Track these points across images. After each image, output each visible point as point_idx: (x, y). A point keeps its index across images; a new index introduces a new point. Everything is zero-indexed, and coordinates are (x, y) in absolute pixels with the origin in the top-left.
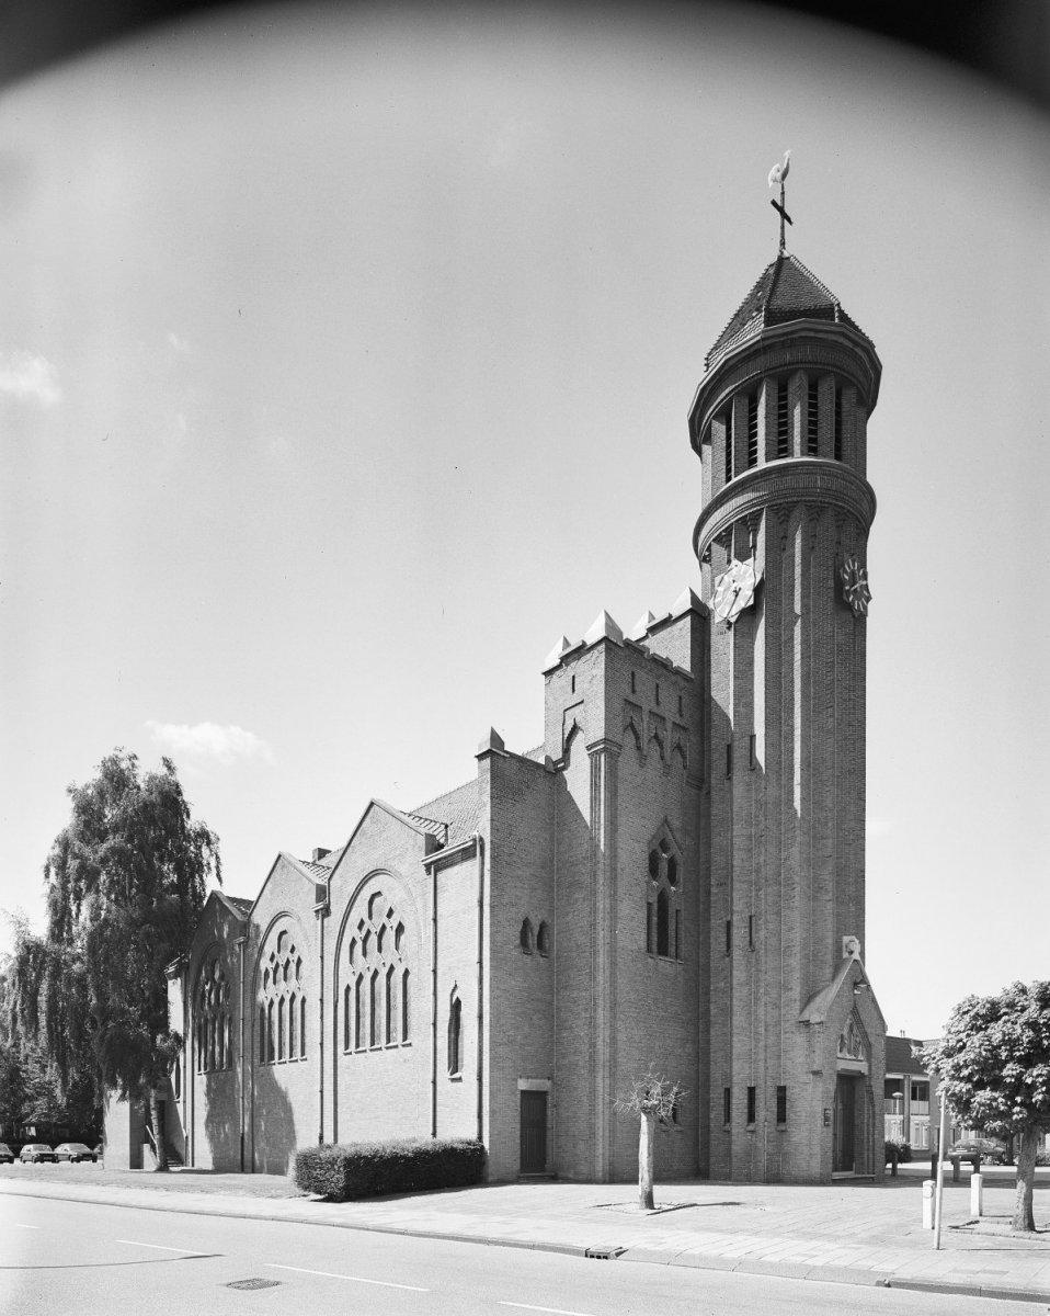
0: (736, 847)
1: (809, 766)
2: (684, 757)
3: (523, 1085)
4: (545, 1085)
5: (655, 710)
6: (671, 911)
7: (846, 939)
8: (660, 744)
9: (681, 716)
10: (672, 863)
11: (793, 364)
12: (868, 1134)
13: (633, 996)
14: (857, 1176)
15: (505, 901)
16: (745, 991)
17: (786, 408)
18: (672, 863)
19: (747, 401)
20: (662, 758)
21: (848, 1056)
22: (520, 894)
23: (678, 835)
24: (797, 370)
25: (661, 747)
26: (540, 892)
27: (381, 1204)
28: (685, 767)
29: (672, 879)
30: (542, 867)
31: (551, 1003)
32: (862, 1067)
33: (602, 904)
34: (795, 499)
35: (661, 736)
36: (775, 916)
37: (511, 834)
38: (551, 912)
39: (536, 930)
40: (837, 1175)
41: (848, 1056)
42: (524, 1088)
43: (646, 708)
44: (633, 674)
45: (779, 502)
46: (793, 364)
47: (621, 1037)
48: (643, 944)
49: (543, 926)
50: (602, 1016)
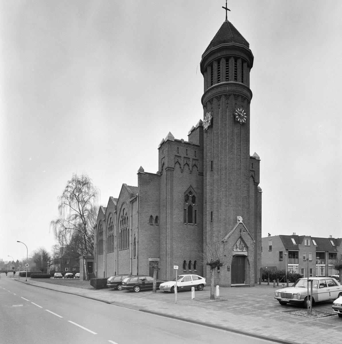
0: (207, 193)
1: (226, 169)
2: (197, 168)
3: (150, 259)
4: (158, 260)
5: (186, 156)
6: (193, 210)
7: (238, 217)
8: (188, 165)
9: (196, 156)
10: (194, 197)
11: (220, 56)
12: (248, 273)
13: (179, 235)
14: (245, 285)
15: (144, 211)
16: (210, 232)
17: (228, 64)
18: (194, 197)
19: (211, 67)
20: (189, 169)
21: (239, 250)
22: (149, 209)
23: (195, 190)
24: (213, 62)
25: (189, 166)
26: (156, 208)
27: (76, 288)
28: (198, 170)
29: (194, 201)
30: (157, 201)
31: (159, 238)
32: (245, 254)
33: (169, 211)
34: (221, 94)
35: (188, 163)
36: (216, 212)
37: (146, 194)
38: (160, 213)
39: (154, 218)
40: (232, 285)
41: (239, 250)
42: (150, 260)
43: (182, 156)
44: (178, 148)
45: (217, 95)
46: (220, 56)
47: (175, 247)
48: (182, 220)
49: (157, 217)
50: (168, 241)
